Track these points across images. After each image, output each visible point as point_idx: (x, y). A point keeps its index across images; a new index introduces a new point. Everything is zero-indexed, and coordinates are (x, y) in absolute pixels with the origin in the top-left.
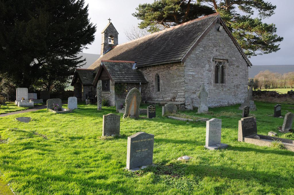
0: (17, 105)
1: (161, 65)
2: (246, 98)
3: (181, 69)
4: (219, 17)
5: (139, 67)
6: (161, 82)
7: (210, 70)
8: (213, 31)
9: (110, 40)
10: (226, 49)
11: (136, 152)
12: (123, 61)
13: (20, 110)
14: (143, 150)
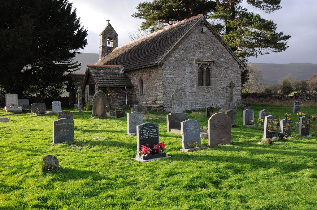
0: (6, 111)
1: (143, 68)
2: (238, 101)
3: (160, 73)
4: (203, 19)
5: (125, 72)
6: (144, 85)
7: (193, 72)
8: (196, 34)
9: (109, 43)
10: (211, 51)
11: (59, 132)
12: (110, 66)
13: (7, 115)
14: (65, 131)
